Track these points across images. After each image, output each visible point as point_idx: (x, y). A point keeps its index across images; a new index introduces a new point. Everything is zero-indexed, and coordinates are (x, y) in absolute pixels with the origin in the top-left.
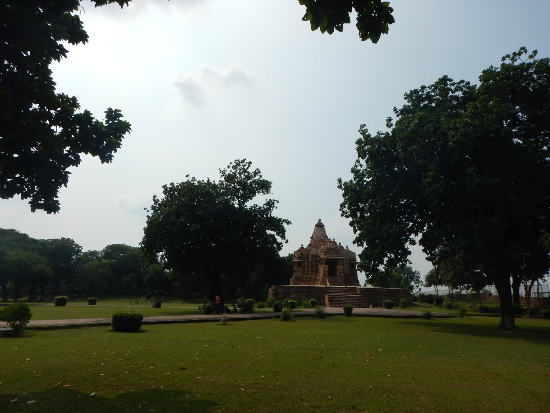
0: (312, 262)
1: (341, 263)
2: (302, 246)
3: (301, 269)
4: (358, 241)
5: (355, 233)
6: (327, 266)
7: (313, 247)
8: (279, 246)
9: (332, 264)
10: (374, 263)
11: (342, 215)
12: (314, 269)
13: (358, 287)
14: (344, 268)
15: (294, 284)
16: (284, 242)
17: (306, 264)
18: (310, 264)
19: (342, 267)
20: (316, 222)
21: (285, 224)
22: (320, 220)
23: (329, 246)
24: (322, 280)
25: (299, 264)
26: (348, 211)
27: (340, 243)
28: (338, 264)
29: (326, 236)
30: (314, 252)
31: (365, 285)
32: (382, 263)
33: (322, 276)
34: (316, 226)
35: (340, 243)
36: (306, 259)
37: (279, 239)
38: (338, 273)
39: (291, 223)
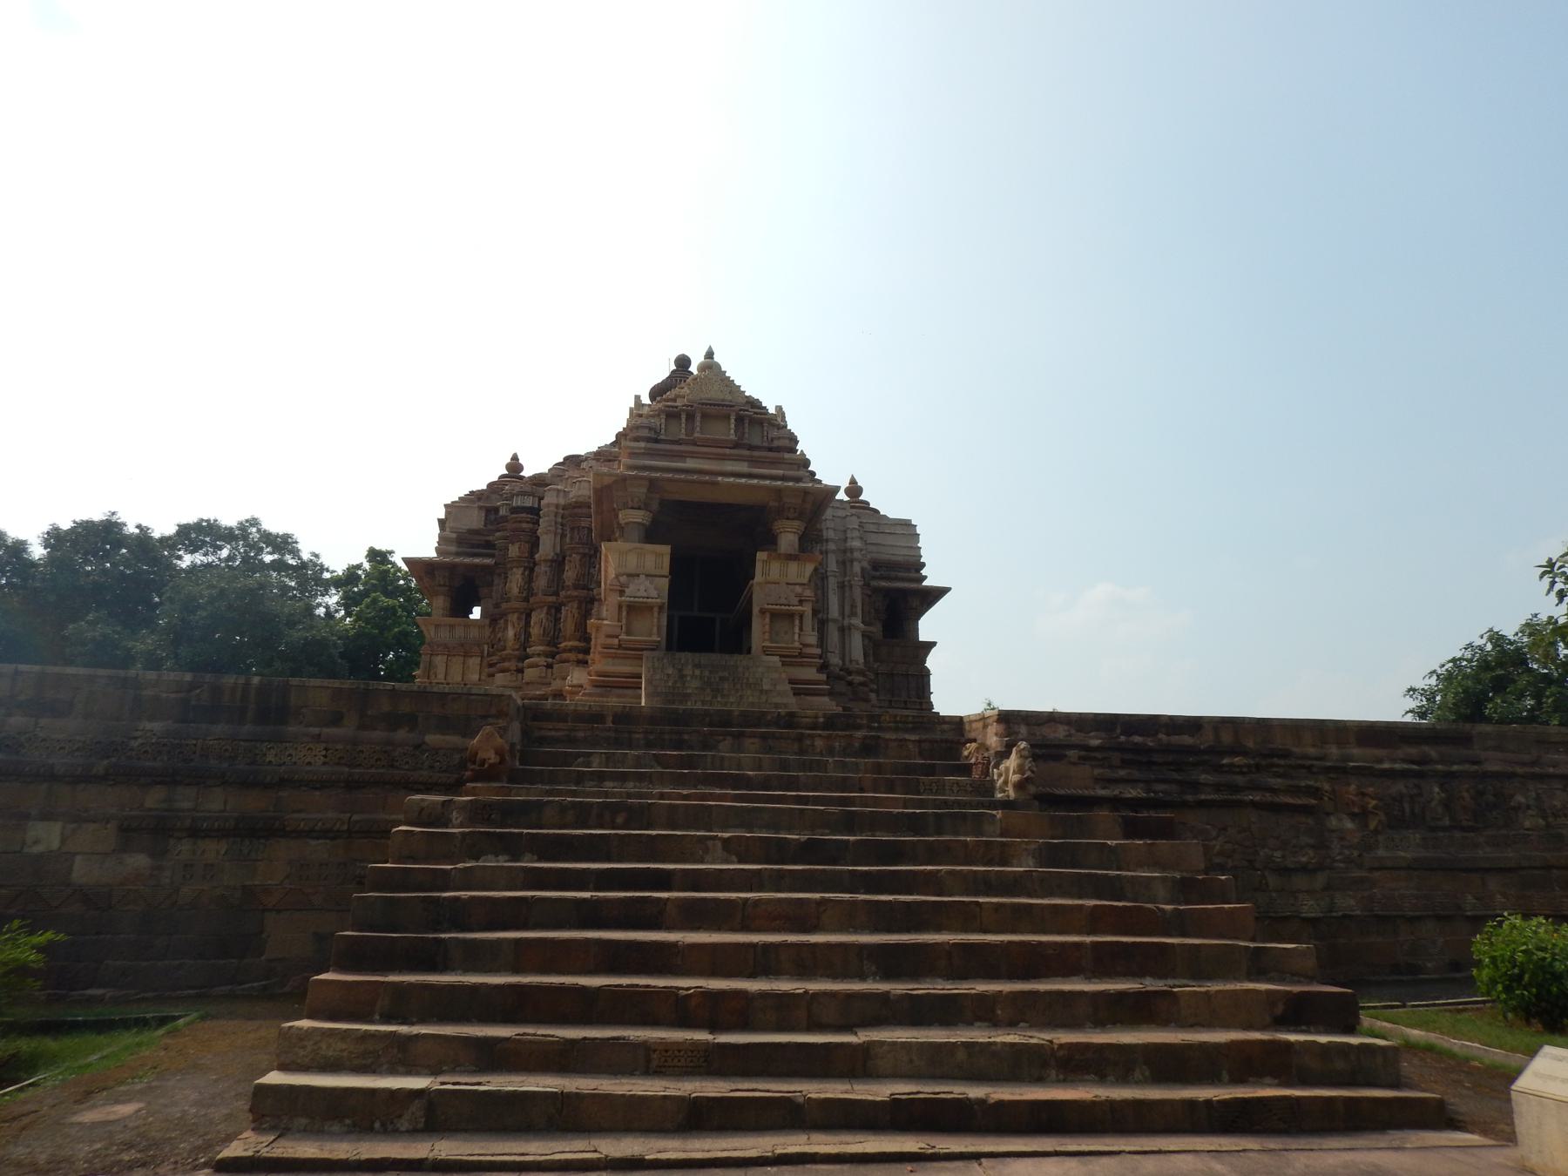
0: (558, 563)
1: (788, 539)
14: (820, 578)
19: (800, 572)
28: (770, 541)
36: (514, 551)
38: (759, 628)
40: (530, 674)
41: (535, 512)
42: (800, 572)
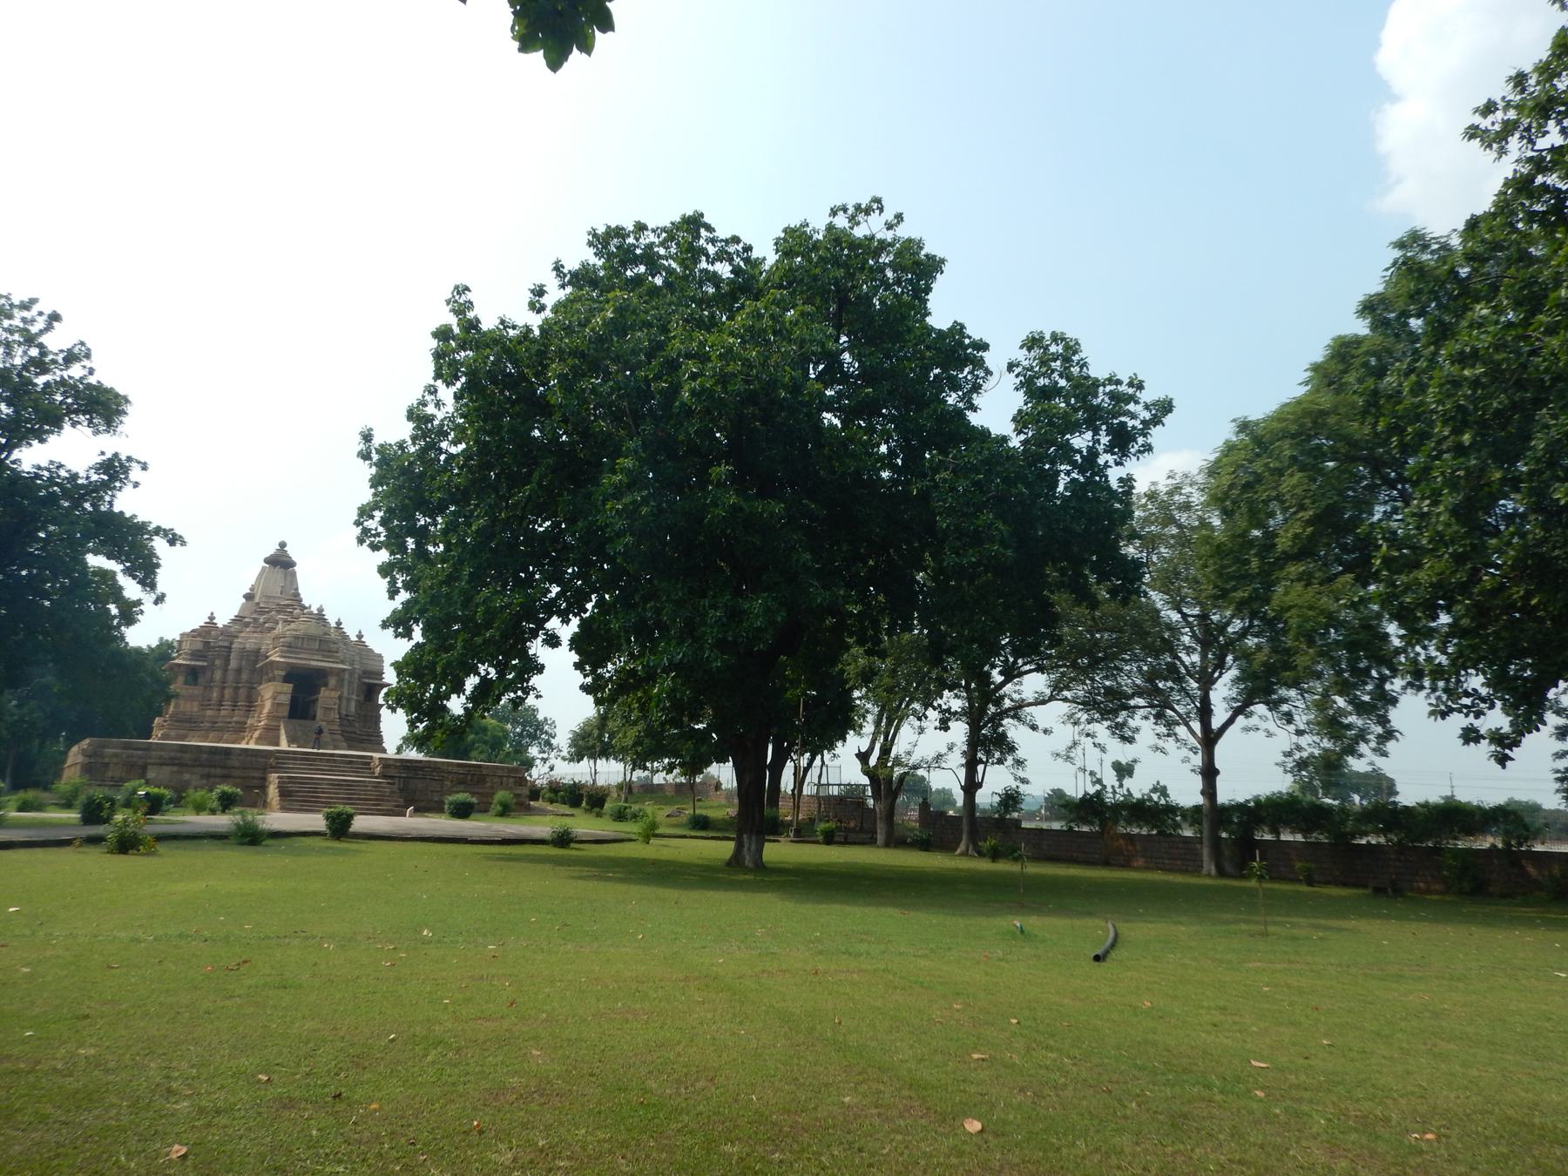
0: (239, 671)
1: (332, 682)
2: (212, 618)
4: (399, 623)
5: (392, 597)
6: (288, 687)
7: (247, 625)
8: (130, 613)
9: (304, 687)
10: (437, 690)
11: (361, 541)
12: (243, 692)
13: (377, 755)
14: (340, 698)
15: (164, 737)
16: (148, 599)
17: (218, 675)
18: (231, 677)
19: (336, 694)
20: (271, 549)
21: (159, 544)
22: (283, 545)
23: (299, 627)
24: (267, 729)
25: (193, 674)
26: (381, 529)
27: (339, 623)
28: (326, 685)
29: (296, 596)
30: (248, 640)
31: (399, 750)
32: (458, 688)
33: (269, 717)
34: (267, 561)
35: (339, 623)
36: (217, 662)
37: (131, 589)
39: (183, 543)
41: (229, 648)
42: (336, 694)
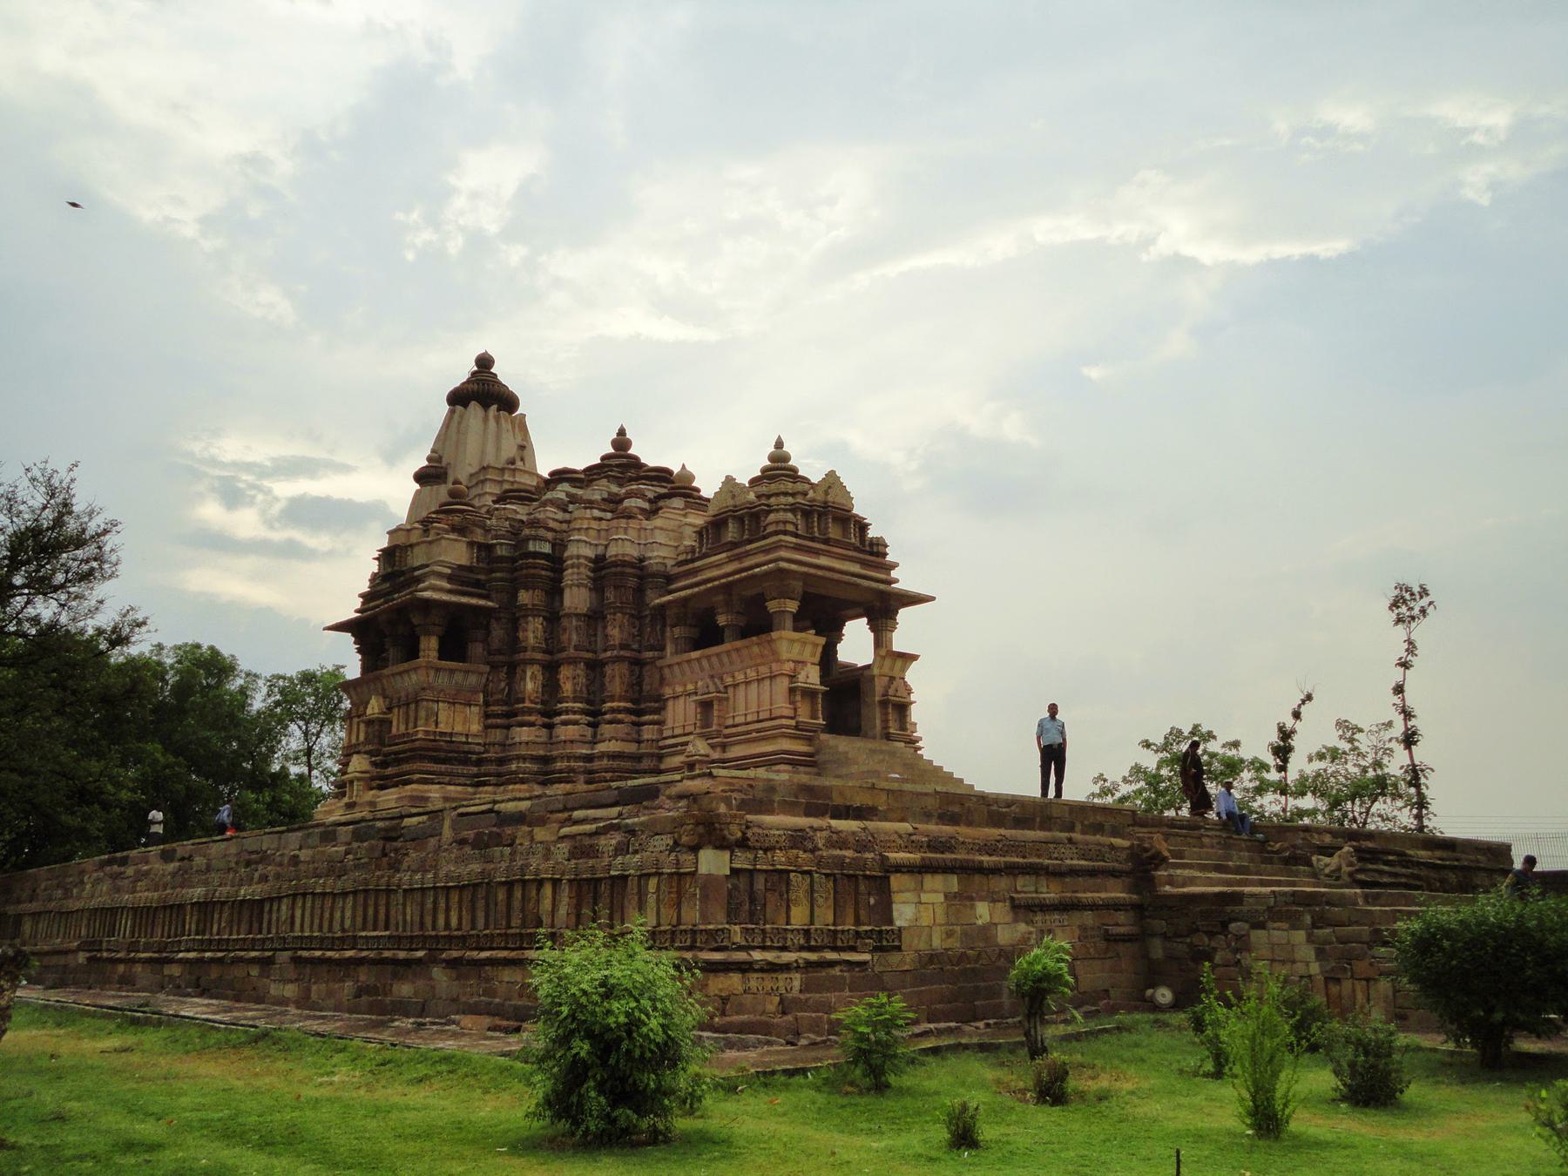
0: (595, 618)
3: (470, 676)
17: (533, 632)
18: (572, 636)
40: (564, 733)
